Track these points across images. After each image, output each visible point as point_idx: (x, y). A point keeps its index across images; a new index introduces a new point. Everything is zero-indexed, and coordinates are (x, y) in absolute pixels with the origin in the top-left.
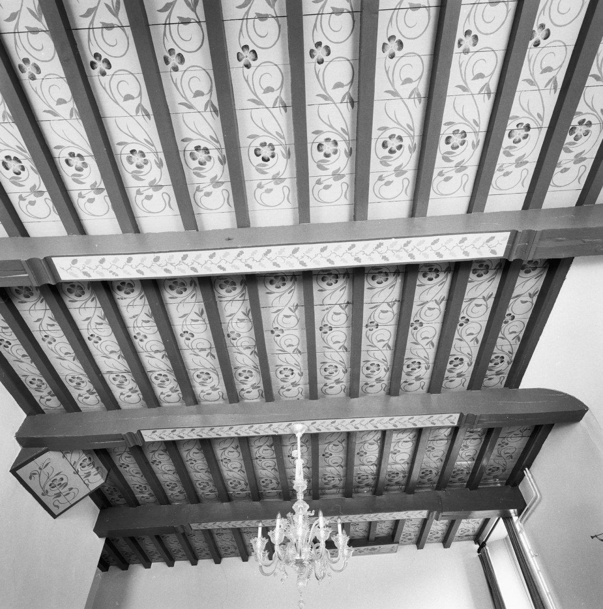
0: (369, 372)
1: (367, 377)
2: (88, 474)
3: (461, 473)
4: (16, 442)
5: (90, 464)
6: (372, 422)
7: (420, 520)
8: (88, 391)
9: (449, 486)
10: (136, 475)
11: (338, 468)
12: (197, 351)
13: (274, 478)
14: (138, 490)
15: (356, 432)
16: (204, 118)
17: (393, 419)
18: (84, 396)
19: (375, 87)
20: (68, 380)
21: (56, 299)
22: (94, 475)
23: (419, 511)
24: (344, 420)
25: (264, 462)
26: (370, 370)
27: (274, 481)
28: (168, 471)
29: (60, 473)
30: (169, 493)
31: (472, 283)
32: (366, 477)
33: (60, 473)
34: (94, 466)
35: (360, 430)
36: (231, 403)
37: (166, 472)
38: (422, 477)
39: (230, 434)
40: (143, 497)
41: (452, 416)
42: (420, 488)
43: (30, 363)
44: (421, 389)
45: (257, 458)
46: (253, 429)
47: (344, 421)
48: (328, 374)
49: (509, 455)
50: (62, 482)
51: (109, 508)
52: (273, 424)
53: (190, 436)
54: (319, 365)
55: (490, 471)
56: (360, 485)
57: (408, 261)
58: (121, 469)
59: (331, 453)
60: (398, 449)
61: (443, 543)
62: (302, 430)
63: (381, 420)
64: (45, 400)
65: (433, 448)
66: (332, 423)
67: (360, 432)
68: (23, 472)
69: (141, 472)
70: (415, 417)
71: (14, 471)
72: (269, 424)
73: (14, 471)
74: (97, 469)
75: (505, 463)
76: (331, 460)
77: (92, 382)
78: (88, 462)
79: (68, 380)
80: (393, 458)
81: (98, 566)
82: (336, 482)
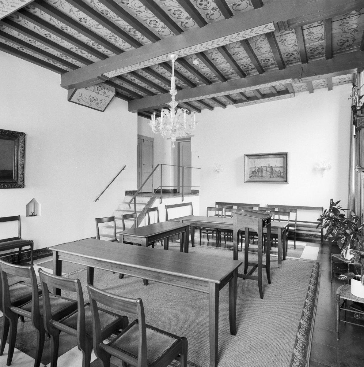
0: (203, 6)
1: (204, 10)
2: (105, 93)
4: (63, 88)
5: (102, 88)
6: (267, 27)
8: (162, 27)
10: (203, 68)
11: (270, 54)
12: (96, 26)
15: (207, 50)
17: (239, 34)
18: (161, 31)
20: (148, 24)
21: (23, 14)
24: (260, 26)
26: (203, 5)
28: (223, 62)
32: (248, 65)
34: (104, 89)
35: (210, 48)
36: (201, 28)
37: (202, 68)
38: (341, 46)
39: (226, 43)
41: (267, 25)
42: (290, 63)
43: (103, 28)
44: (249, 6)
46: (227, 39)
47: (260, 28)
48: (204, 7)
49: (353, 30)
50: (95, 99)
51: (132, 100)
52: (181, 50)
53: (201, 50)
54: (168, 13)
55: (342, 44)
56: (267, 65)
60: (259, 46)
62: (175, 58)
63: (219, 40)
64: (161, 32)
65: (285, 40)
66: (238, 35)
67: (210, 50)
68: (74, 99)
69: (205, 66)
70: (241, 33)
71: (69, 100)
72: (201, 44)
73: (69, 100)
74: (108, 89)
75: (352, 36)
76: (263, 51)
77: (162, 21)
78: (100, 88)
79: (148, 24)
80: (259, 52)
81: (138, 115)
82: (272, 61)
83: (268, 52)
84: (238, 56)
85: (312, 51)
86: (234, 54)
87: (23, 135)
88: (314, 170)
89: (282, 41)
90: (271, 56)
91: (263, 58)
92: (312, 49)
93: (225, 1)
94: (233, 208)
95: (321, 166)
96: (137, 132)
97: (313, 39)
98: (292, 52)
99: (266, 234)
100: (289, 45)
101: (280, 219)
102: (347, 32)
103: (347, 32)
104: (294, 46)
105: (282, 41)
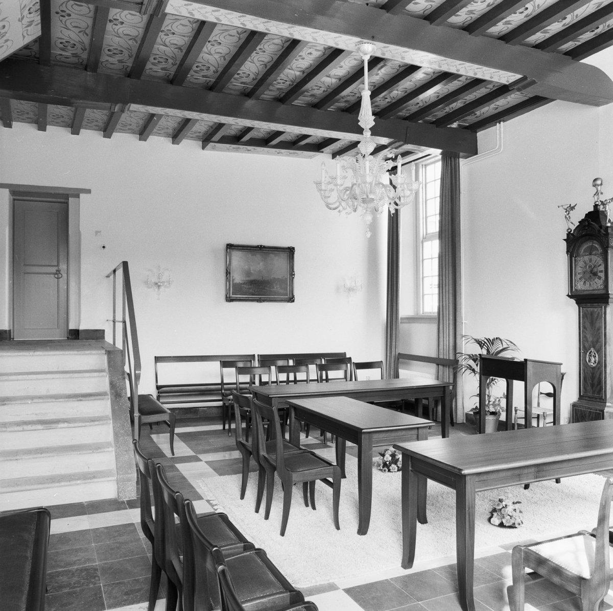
3: (283, 83)
7: (180, 120)
9: (334, 109)
13: (172, 58)
14: (61, 46)
16: (73, 427)
19: (139, 342)
22: (35, 25)
23: (198, 113)
25: (171, 39)
27: (170, 61)
29: (5, 18)
30: (104, 58)
31: (515, 529)
33: (5, 18)
40: (61, 55)
45: (110, 21)
57: (210, 511)
58: (89, 31)
59: (70, 12)
61: (140, 135)
83: (80, 30)
84: (117, 27)
85: (111, 53)
86: (57, 13)
87: (229, 299)
88: (338, 289)
89: (63, 14)
90: (81, 40)
91: (63, 37)
92: (111, 48)
93: (611, 12)
94: (505, 420)
95: (349, 284)
96: (81, 201)
97: (168, 44)
98: (75, 43)
99: (301, 431)
100: (171, 44)
101: (225, 382)
102: (254, 63)
103: (254, 63)
104: (82, 33)
105: (63, 14)
